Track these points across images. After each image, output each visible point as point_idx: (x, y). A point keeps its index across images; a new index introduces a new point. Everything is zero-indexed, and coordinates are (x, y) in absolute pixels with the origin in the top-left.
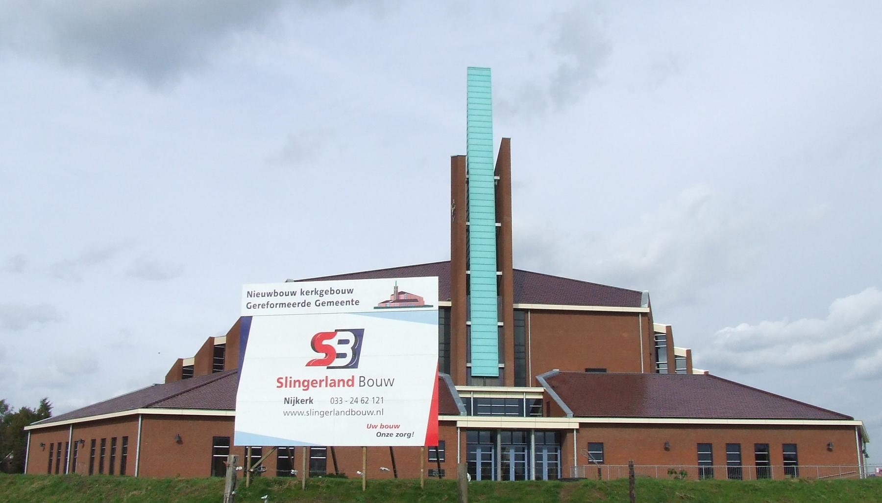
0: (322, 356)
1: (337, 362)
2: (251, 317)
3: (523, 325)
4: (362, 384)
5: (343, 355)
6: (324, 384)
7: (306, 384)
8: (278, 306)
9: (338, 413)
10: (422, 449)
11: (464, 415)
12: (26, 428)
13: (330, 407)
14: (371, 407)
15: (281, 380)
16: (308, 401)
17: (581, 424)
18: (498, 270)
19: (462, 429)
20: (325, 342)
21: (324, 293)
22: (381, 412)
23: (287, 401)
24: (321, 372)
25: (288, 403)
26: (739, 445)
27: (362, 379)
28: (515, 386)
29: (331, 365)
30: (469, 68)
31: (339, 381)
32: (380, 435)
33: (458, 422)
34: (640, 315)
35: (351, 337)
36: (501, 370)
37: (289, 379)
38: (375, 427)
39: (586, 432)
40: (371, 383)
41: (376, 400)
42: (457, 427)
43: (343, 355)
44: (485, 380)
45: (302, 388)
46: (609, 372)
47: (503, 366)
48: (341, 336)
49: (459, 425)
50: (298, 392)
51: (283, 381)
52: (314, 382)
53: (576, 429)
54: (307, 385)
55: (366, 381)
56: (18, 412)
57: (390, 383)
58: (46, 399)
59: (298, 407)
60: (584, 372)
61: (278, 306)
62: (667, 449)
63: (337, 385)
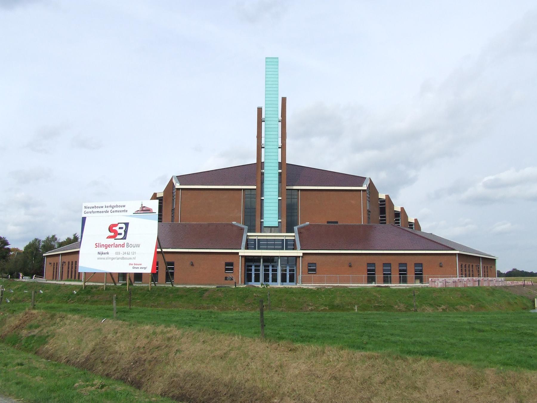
0: (112, 234)
1: (119, 237)
2: (86, 217)
3: (297, 198)
4: (128, 246)
5: (121, 234)
6: (113, 246)
7: (106, 246)
8: (96, 212)
9: (118, 259)
10: (150, 274)
11: (243, 249)
12: (44, 255)
13: (115, 256)
14: (131, 256)
15: (96, 244)
16: (107, 253)
17: (303, 253)
18: (279, 169)
19: (242, 256)
20: (114, 228)
21: (114, 207)
22: (134, 258)
23: (99, 253)
24: (112, 241)
25: (99, 254)
26: (390, 264)
27: (128, 244)
28: (286, 233)
29: (116, 238)
30: (266, 58)
31: (119, 245)
32: (134, 268)
33: (239, 253)
34: (362, 191)
35: (124, 226)
36: (280, 223)
37: (100, 244)
38: (132, 264)
39: (307, 258)
40: (131, 246)
41: (133, 253)
42: (240, 256)
43: (121, 234)
44: (271, 229)
45: (105, 248)
46: (339, 224)
47: (281, 221)
48: (120, 225)
49: (240, 254)
50: (103, 250)
51: (98, 245)
52: (109, 245)
53: (302, 256)
54: (107, 246)
55: (129, 245)
56: (66, 240)
57: (138, 246)
58: (76, 234)
59: (103, 256)
60: (326, 224)
61: (96, 212)
62: (350, 266)
63: (118, 247)
